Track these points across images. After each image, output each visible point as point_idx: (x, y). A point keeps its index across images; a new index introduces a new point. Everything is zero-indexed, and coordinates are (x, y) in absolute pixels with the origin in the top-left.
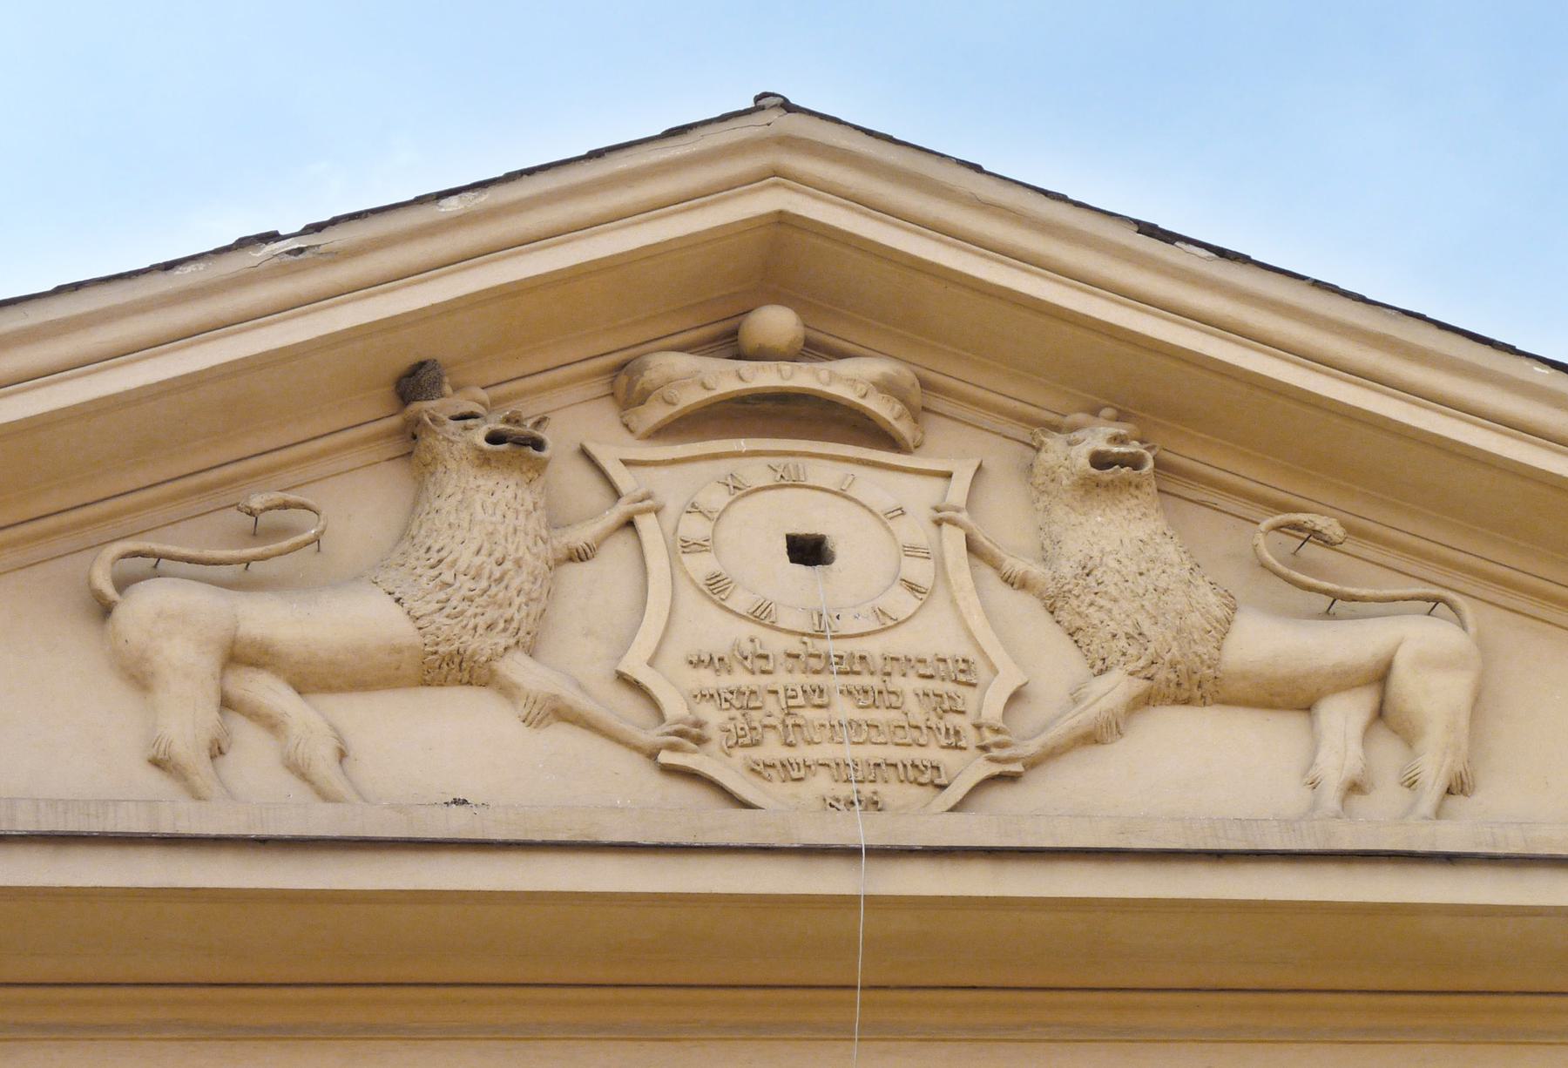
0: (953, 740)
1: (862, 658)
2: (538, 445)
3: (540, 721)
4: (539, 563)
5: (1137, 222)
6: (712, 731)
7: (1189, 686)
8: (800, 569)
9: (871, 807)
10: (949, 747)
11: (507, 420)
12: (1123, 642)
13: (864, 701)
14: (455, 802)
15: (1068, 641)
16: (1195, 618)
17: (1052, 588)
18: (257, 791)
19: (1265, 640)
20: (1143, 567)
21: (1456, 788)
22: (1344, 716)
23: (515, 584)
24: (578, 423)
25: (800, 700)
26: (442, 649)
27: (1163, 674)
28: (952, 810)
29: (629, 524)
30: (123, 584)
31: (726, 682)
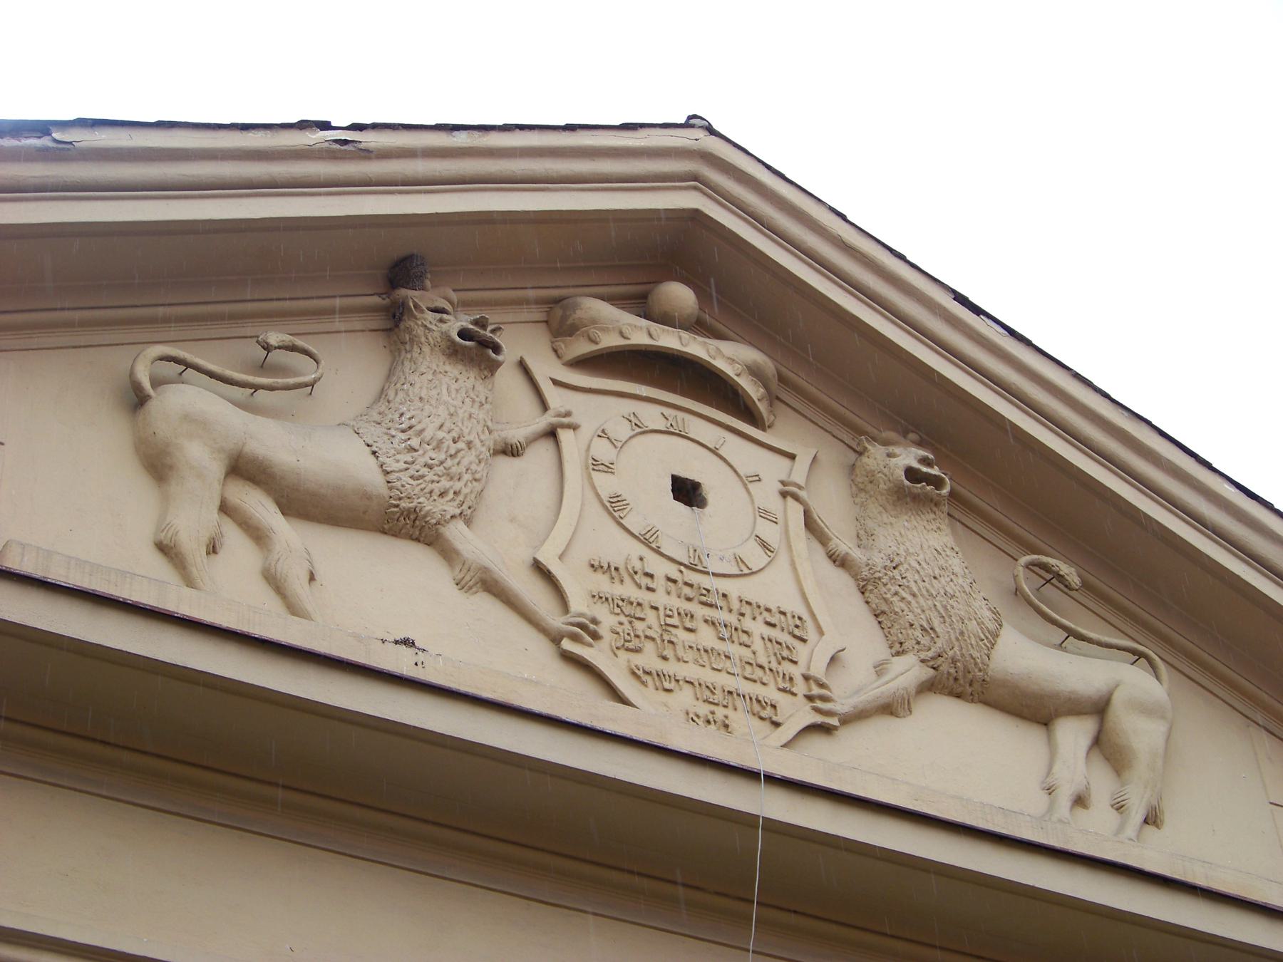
0: (787, 685)
1: (724, 596)
2: (497, 349)
3: (471, 588)
4: (484, 449)
5: (954, 291)
6: (603, 630)
8: (680, 506)
10: (784, 690)
11: (476, 323)
12: (918, 633)
15: (872, 622)
16: (972, 626)
17: (865, 573)
18: (232, 590)
19: (1023, 655)
20: (937, 572)
21: (1152, 819)
22: (1073, 735)
23: (465, 462)
24: (521, 342)
25: (675, 621)
26: (403, 504)
27: (945, 668)
28: (784, 746)
29: (551, 434)
30: (157, 383)
31: (618, 590)
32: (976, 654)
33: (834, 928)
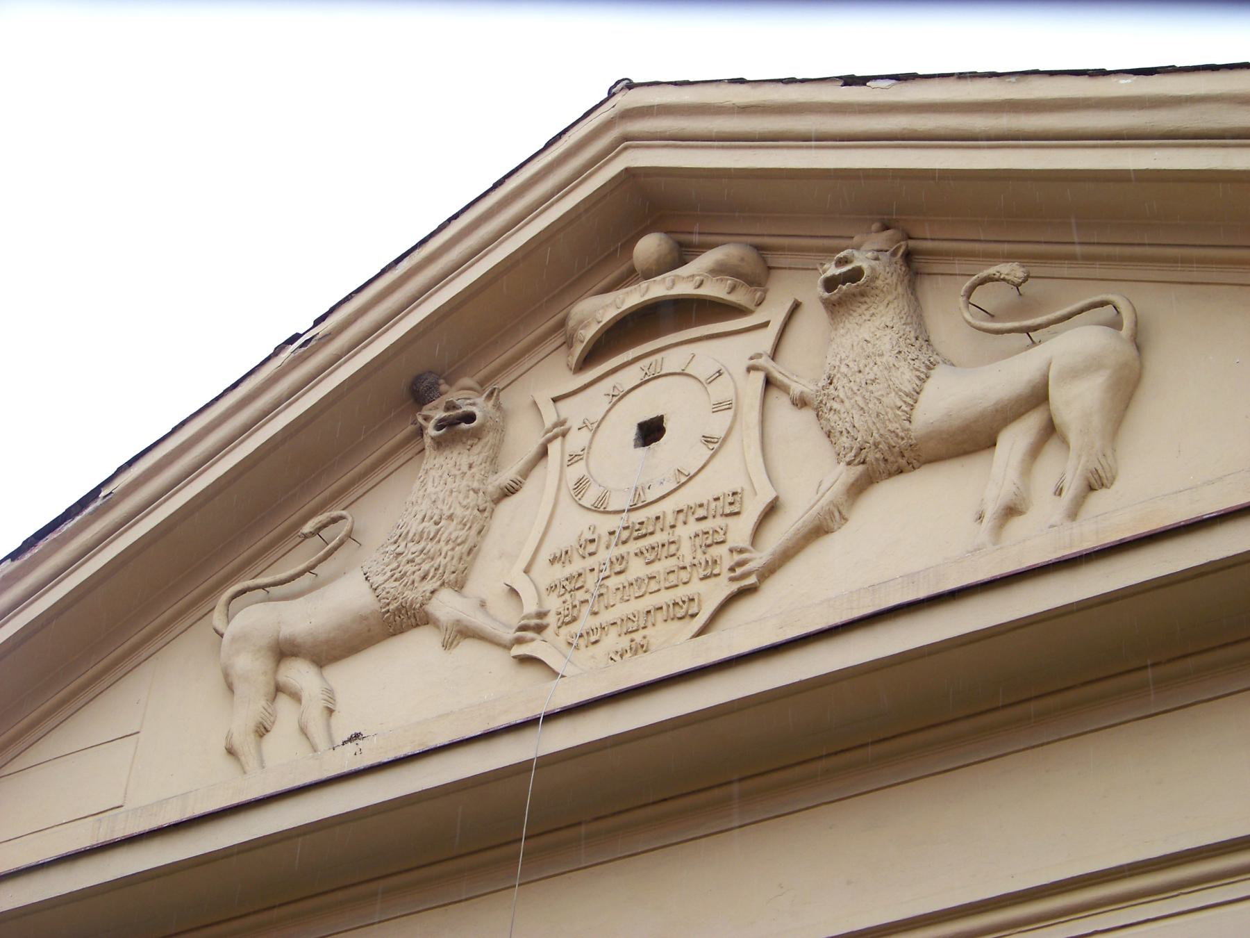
5: (840, 78)
7: (890, 460)
9: (640, 651)
11: (447, 409)
13: (650, 556)
14: (350, 740)
18: (285, 762)
19: (951, 395)
26: (391, 607)
27: (871, 456)
32: (892, 427)
33: (798, 770)
